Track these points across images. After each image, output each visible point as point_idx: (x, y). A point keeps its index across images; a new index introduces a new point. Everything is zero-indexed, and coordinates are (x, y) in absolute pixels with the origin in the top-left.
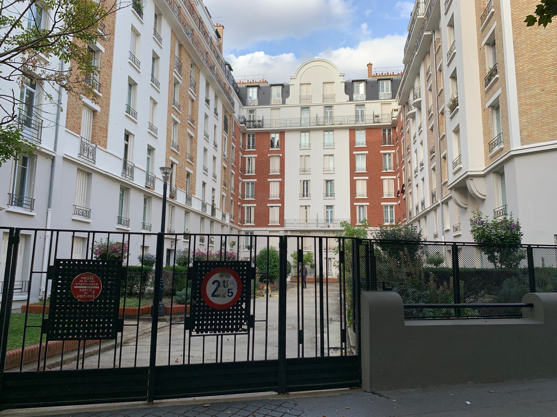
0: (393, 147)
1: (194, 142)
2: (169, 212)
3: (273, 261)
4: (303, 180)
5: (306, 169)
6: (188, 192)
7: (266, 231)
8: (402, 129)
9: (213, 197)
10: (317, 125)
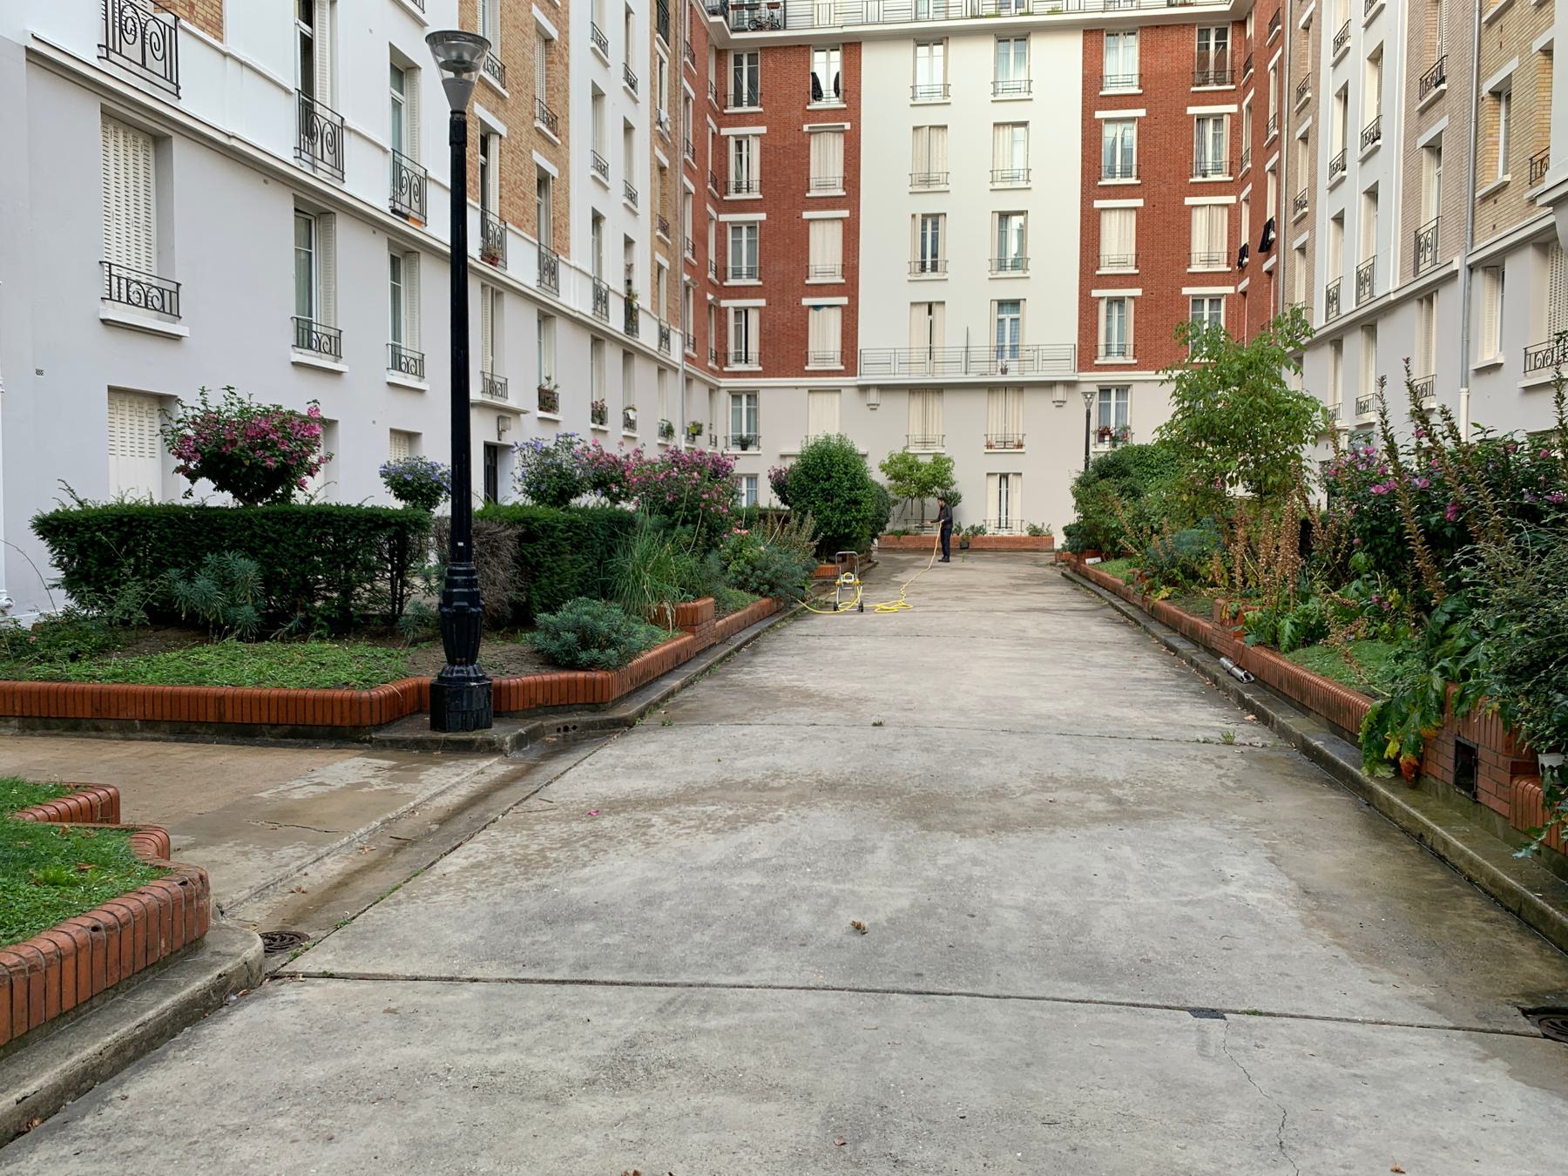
0: (1231, 95)
1: (556, 60)
2: (484, 315)
3: (846, 484)
4: (923, 215)
5: (934, 176)
6: (543, 242)
7: (796, 388)
8: (1276, 20)
9: (629, 268)
10: (973, 17)
